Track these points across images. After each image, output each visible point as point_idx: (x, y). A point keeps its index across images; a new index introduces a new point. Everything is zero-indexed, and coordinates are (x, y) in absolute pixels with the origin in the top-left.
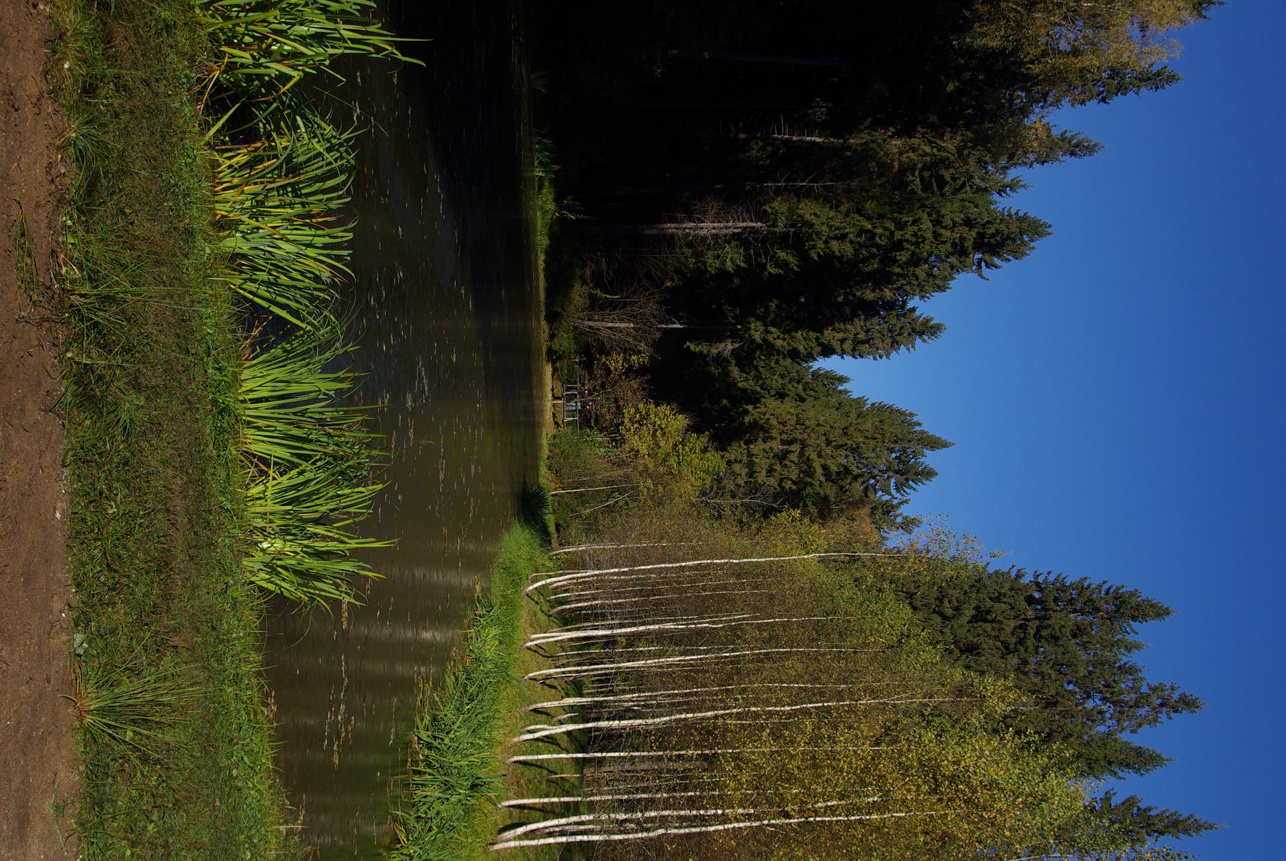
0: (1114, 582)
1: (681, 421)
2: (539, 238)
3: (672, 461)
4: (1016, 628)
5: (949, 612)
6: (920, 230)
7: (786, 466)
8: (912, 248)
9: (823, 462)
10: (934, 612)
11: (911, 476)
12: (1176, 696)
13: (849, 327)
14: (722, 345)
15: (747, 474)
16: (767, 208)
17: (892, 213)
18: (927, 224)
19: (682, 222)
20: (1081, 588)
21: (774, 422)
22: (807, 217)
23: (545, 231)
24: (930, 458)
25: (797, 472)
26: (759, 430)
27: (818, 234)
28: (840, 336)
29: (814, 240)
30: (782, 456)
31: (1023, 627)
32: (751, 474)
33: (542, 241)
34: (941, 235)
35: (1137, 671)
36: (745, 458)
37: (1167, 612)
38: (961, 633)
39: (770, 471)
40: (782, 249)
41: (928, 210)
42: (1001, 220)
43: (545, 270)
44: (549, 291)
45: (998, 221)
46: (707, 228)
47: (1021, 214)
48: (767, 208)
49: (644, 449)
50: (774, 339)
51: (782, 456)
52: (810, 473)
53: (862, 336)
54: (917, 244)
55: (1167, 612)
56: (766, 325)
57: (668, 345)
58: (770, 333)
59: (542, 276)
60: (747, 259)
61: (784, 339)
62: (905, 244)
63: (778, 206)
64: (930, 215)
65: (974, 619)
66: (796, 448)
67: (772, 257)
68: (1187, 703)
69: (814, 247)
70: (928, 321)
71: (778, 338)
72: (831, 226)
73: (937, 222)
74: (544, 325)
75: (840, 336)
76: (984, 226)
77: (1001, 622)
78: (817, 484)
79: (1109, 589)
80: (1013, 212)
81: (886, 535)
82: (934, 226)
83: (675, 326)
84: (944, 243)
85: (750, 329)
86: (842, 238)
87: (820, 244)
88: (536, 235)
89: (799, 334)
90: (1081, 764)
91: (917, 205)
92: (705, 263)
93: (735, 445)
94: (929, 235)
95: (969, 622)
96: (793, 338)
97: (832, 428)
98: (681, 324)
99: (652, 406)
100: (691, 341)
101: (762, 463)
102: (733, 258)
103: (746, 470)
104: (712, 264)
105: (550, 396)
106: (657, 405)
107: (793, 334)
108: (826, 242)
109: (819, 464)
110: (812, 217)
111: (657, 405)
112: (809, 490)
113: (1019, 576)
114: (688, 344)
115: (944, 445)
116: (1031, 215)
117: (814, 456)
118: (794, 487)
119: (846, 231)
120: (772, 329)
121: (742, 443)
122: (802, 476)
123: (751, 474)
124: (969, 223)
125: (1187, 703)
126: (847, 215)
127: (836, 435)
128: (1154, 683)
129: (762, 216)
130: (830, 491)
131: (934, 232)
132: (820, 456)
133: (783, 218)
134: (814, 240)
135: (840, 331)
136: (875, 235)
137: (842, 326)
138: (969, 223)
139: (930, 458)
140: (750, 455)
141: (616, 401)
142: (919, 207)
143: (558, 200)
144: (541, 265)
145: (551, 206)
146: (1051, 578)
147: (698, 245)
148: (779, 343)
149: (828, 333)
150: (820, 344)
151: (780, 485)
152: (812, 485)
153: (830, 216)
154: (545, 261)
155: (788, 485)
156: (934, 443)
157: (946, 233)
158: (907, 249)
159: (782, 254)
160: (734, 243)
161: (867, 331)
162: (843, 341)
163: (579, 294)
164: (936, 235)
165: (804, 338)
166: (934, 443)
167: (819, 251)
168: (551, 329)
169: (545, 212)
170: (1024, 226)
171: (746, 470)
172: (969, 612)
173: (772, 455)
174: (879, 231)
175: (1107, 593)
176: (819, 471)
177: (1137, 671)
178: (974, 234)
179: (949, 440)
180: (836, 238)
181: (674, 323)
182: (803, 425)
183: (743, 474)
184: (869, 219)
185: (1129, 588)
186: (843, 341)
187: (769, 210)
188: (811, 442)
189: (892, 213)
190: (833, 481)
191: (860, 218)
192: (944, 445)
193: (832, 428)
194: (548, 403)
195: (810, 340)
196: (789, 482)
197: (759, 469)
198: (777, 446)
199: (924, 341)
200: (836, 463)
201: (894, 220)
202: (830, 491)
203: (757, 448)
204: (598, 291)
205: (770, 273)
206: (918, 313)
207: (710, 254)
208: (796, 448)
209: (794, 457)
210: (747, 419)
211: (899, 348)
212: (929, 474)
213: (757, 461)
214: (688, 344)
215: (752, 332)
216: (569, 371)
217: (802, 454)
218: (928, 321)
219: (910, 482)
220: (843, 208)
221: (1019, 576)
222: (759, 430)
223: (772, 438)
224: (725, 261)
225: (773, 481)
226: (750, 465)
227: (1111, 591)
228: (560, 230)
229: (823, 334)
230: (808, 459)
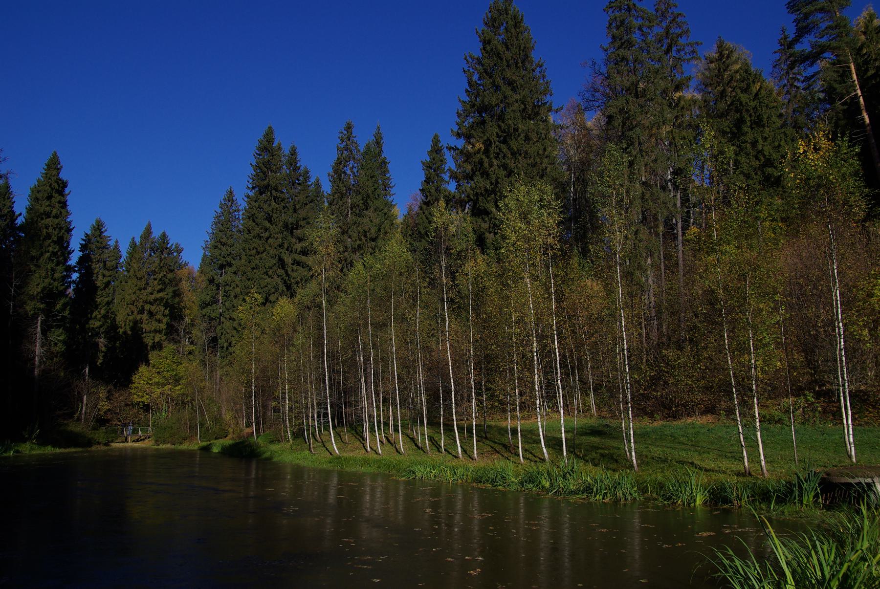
0: (254, 150)
1: (143, 369)
2: (47, 451)
3: (167, 375)
4: (275, 202)
5: (267, 234)
6: (52, 226)
7: (156, 312)
8: (63, 231)
9: (156, 292)
10: (266, 241)
11: (165, 246)
12: (346, 132)
13: (96, 271)
14: (100, 344)
15: (159, 334)
16: (30, 314)
17: (40, 240)
18: (48, 221)
19: (34, 364)
20: (257, 167)
21: (131, 318)
22: (39, 290)
23: (43, 448)
24: (156, 234)
25: (160, 307)
26: (136, 326)
27: (50, 284)
28: (100, 277)
29: (53, 288)
30: (151, 314)
31: (275, 198)
32: (160, 332)
33: (49, 450)
34: (56, 214)
35: (294, 147)
36: (152, 334)
37: (270, 128)
38: (277, 230)
39: (159, 321)
40: (54, 306)
41: (39, 220)
42: (50, 179)
43: (65, 448)
44: (77, 445)
45: (50, 181)
46: (38, 350)
47: (46, 167)
48: (30, 314)
49: (159, 391)
50: (100, 314)
51: (151, 314)
52: (162, 299)
53: (102, 265)
54: (61, 228)
55: (270, 128)
56: (91, 318)
57: (98, 374)
58: (96, 316)
59: (67, 450)
60: (58, 327)
61: (101, 309)
62: (59, 235)
63: (30, 307)
64: (42, 219)
65: (270, 222)
66: (147, 307)
67: (59, 312)
68: (349, 128)
69: (57, 287)
70: (94, 227)
71: (99, 312)
72: (45, 277)
73: (48, 215)
74: (94, 448)
75: (100, 277)
76: (52, 189)
77: (273, 209)
78: (167, 297)
79: (256, 154)
80: (44, 171)
81: (184, 262)
82: (50, 217)
83: (87, 371)
84: (61, 213)
85: (93, 328)
86: (53, 270)
87: (56, 284)
88: (44, 454)
89: (99, 300)
90: (429, 175)
91: (35, 225)
92: (57, 353)
93: (145, 340)
94: (56, 221)
95: (271, 224)
96: (100, 304)
97: (136, 286)
98: (86, 366)
99: (134, 385)
100: (97, 362)
101: (155, 325)
102: (58, 335)
103: (158, 334)
104: (60, 348)
105: (126, 444)
106: (132, 383)
107: (98, 303)
108: (55, 280)
109: (157, 295)
110: (39, 287)
111: (132, 383)
112: (169, 301)
113: (248, 197)
114: (98, 364)
115: (149, 226)
116: (47, 162)
117: (153, 297)
118: (168, 309)
119: (49, 268)
120: (94, 315)
121: (142, 336)
122: (162, 304)
123: (160, 332)
124: (49, 198)
125: (349, 128)
126: (39, 267)
127: (142, 283)
128: (340, 141)
129: (35, 317)
130: (170, 290)
131: (54, 217)
132: (152, 294)
133: (38, 304)
134: (53, 288)
135: (97, 277)
136: (53, 252)
137: (95, 275)
138: (49, 198)
139: (156, 234)
140: (150, 332)
141: (127, 405)
142: (37, 224)
143: (24, 441)
144: (62, 450)
145: (28, 445)
146: (251, 181)
147: (51, 355)
148: (103, 312)
149: (99, 284)
150: (104, 288)
151: (166, 316)
152: (167, 299)
153: (38, 276)
154: (60, 448)
155: (167, 312)
156: (148, 231)
157: (55, 211)
158: (63, 234)
159: (58, 307)
160: (48, 334)
161: (98, 261)
162: (104, 276)
163: (75, 427)
164: (56, 217)
165: (101, 297)
166: (148, 231)
167: (59, 284)
168: (95, 444)
169: (32, 449)
170: (54, 166)
171: (158, 334)
172: (268, 225)
173: (150, 320)
174: (51, 249)
175: (260, 155)
176: (161, 295)
177: (294, 147)
178: (56, 195)
179: (147, 223)
180: (53, 275)
181: (85, 371)
182: (134, 301)
183: (160, 336)
184: (42, 254)
185: (257, 144)
186: (104, 276)
187: (32, 312)
188: (145, 298)
189: (40, 240)
190: (165, 288)
191: (42, 259)
192: (149, 226)
193: (136, 286)
194: (130, 444)
195: (102, 294)
196: (165, 311)
197: (158, 327)
198: (145, 317)
199: (106, 230)
200: (155, 284)
201: (44, 239)
202: (170, 290)
203: (145, 327)
204: (76, 416)
205: (68, 314)
206: (89, 232)
207: (54, 349)
208: (147, 307)
209: (153, 308)
210: (130, 333)
211: (109, 245)
212: (164, 236)
213: (153, 328)
214: (98, 364)
215: (95, 326)
216: (113, 433)
217: (151, 303)
218: (94, 227)
219: (168, 246)
220: (33, 268)
221: (248, 197)
222: (136, 326)
223: (141, 319)
224: (58, 340)
225: (165, 320)
226: (156, 331)
227: (258, 153)
228: (43, 442)
229: (99, 287)
230: (154, 300)
